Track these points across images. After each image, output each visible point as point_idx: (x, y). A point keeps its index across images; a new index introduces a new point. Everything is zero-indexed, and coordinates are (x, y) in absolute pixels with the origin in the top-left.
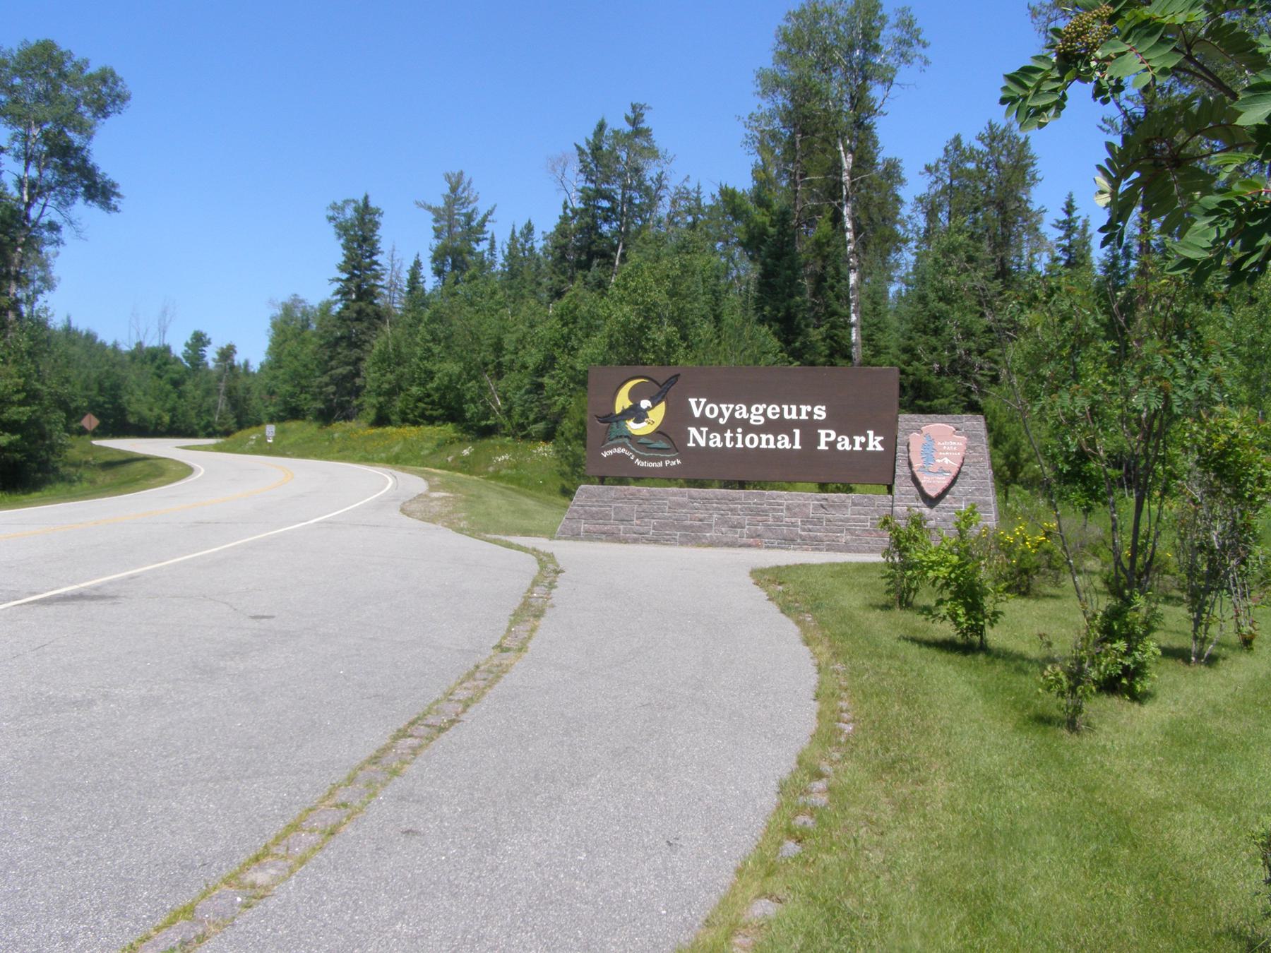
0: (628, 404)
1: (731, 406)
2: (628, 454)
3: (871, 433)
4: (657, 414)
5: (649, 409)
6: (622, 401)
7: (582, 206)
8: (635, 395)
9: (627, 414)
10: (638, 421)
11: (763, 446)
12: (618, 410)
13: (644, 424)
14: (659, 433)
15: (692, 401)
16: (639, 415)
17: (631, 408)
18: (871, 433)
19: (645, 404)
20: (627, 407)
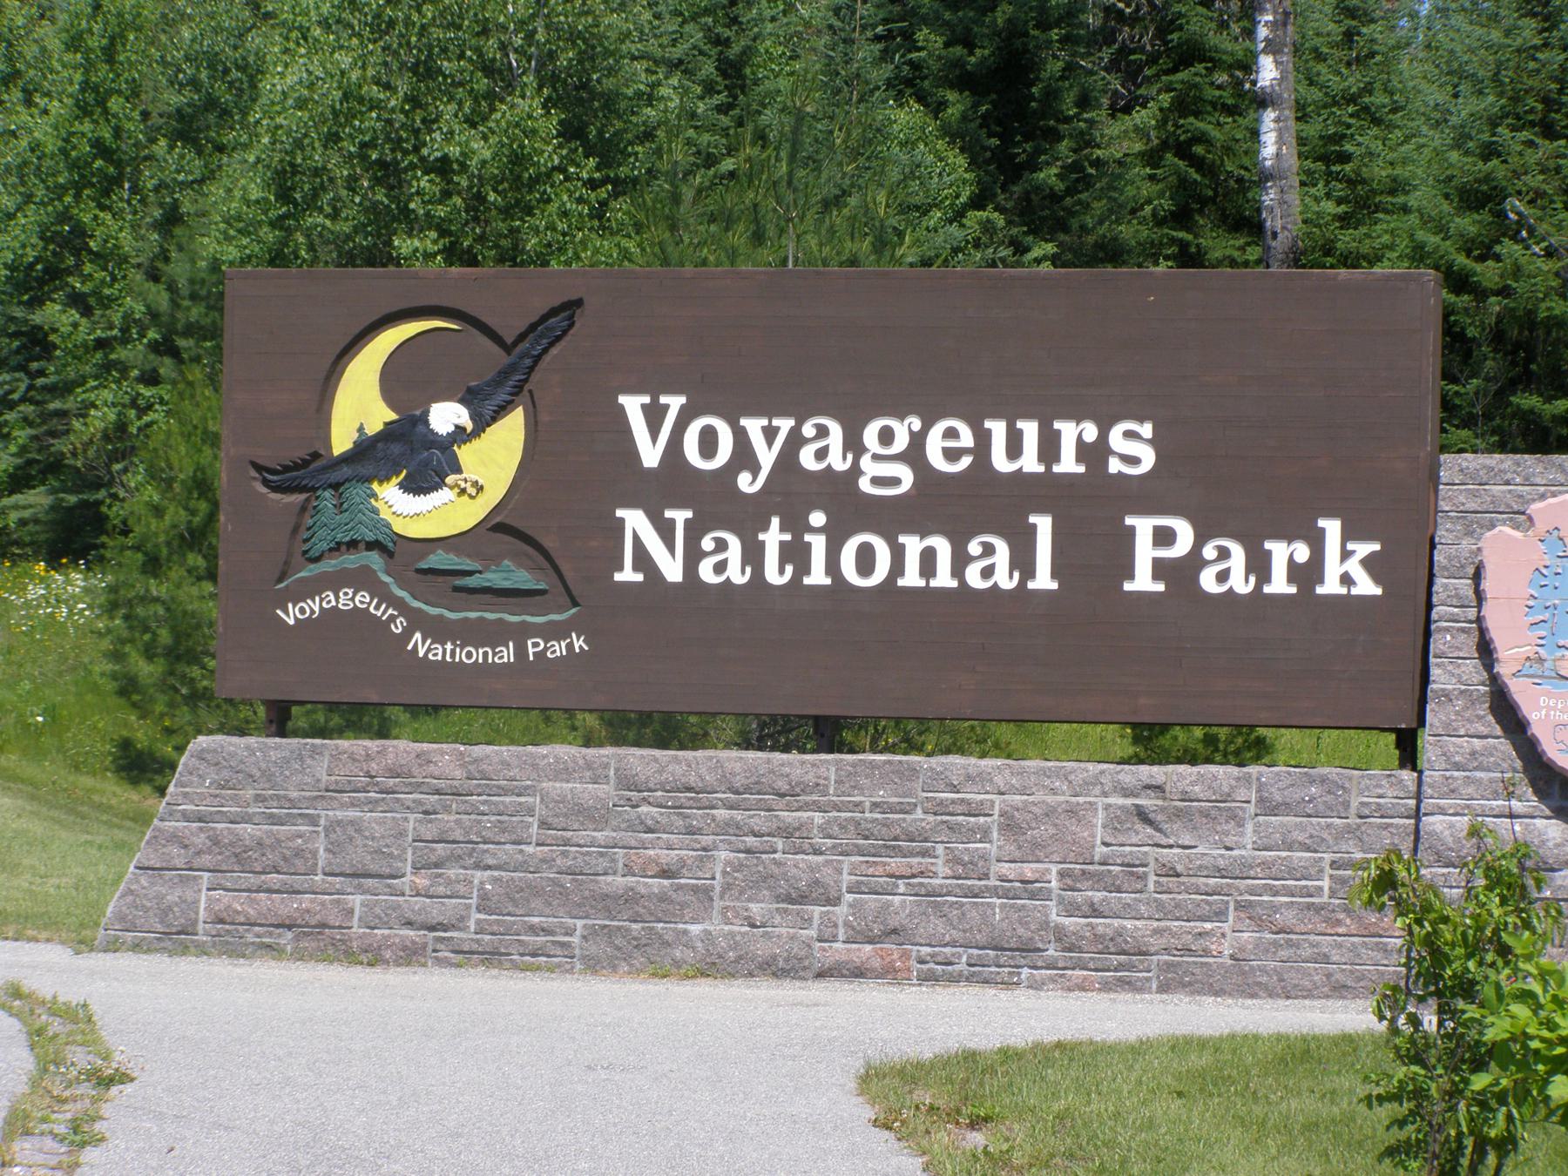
0: (379, 416)
2: (382, 612)
3: (1332, 528)
4: (495, 457)
6: (358, 407)
8: (399, 379)
9: (373, 456)
10: (418, 485)
12: (341, 441)
13: (443, 495)
14: (500, 527)
17: (390, 433)
18: (1332, 528)
19: (446, 416)
20: (374, 427)
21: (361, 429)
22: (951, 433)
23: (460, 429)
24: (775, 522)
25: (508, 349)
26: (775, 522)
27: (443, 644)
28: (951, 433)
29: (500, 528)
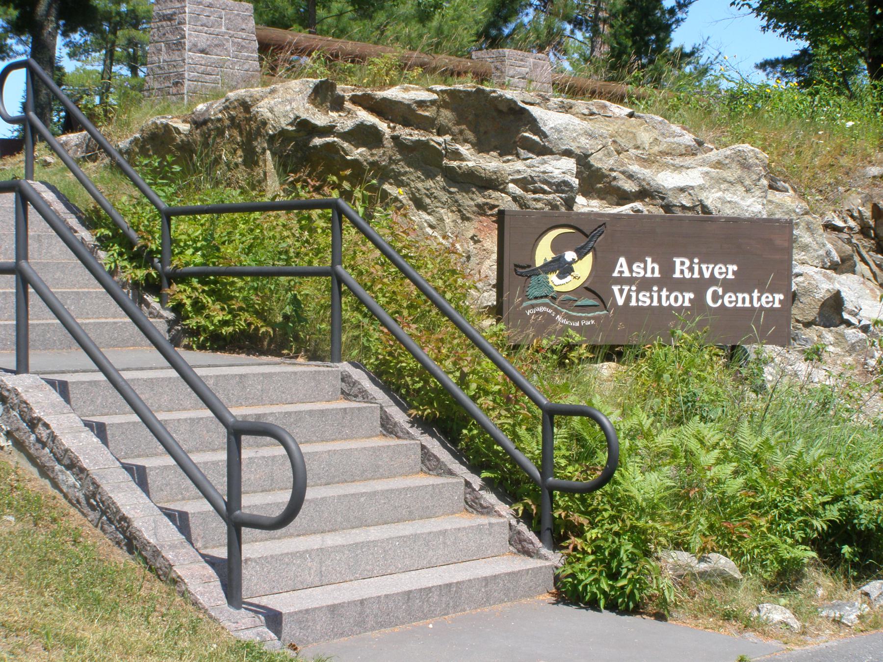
0: (550, 256)
1: (711, 266)
2: (550, 311)
3: (649, 260)
4: (583, 268)
5: (574, 261)
6: (543, 253)
7: (808, 42)
8: (556, 245)
9: (548, 267)
10: (562, 276)
11: (740, 305)
12: (539, 262)
13: (569, 278)
14: (587, 289)
15: (678, 261)
16: (565, 270)
17: (554, 260)
18: (649, 260)
19: (570, 256)
20: (549, 259)
21: (545, 260)
22: (720, 268)
23: (574, 260)
24: (756, 291)
25: (587, 236)
26: (756, 291)
27: (751, 293)
28: (720, 268)
29: (586, 288)
